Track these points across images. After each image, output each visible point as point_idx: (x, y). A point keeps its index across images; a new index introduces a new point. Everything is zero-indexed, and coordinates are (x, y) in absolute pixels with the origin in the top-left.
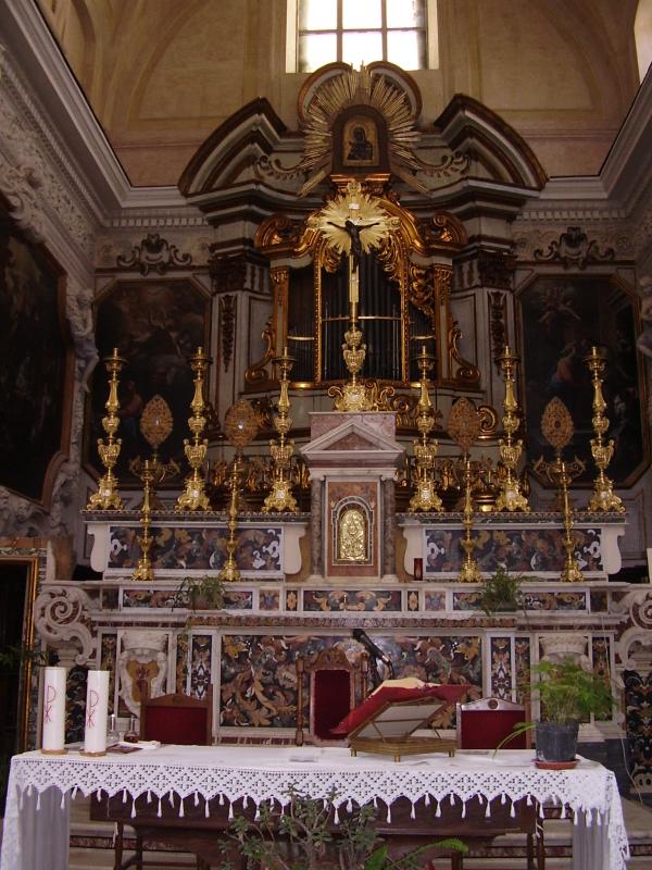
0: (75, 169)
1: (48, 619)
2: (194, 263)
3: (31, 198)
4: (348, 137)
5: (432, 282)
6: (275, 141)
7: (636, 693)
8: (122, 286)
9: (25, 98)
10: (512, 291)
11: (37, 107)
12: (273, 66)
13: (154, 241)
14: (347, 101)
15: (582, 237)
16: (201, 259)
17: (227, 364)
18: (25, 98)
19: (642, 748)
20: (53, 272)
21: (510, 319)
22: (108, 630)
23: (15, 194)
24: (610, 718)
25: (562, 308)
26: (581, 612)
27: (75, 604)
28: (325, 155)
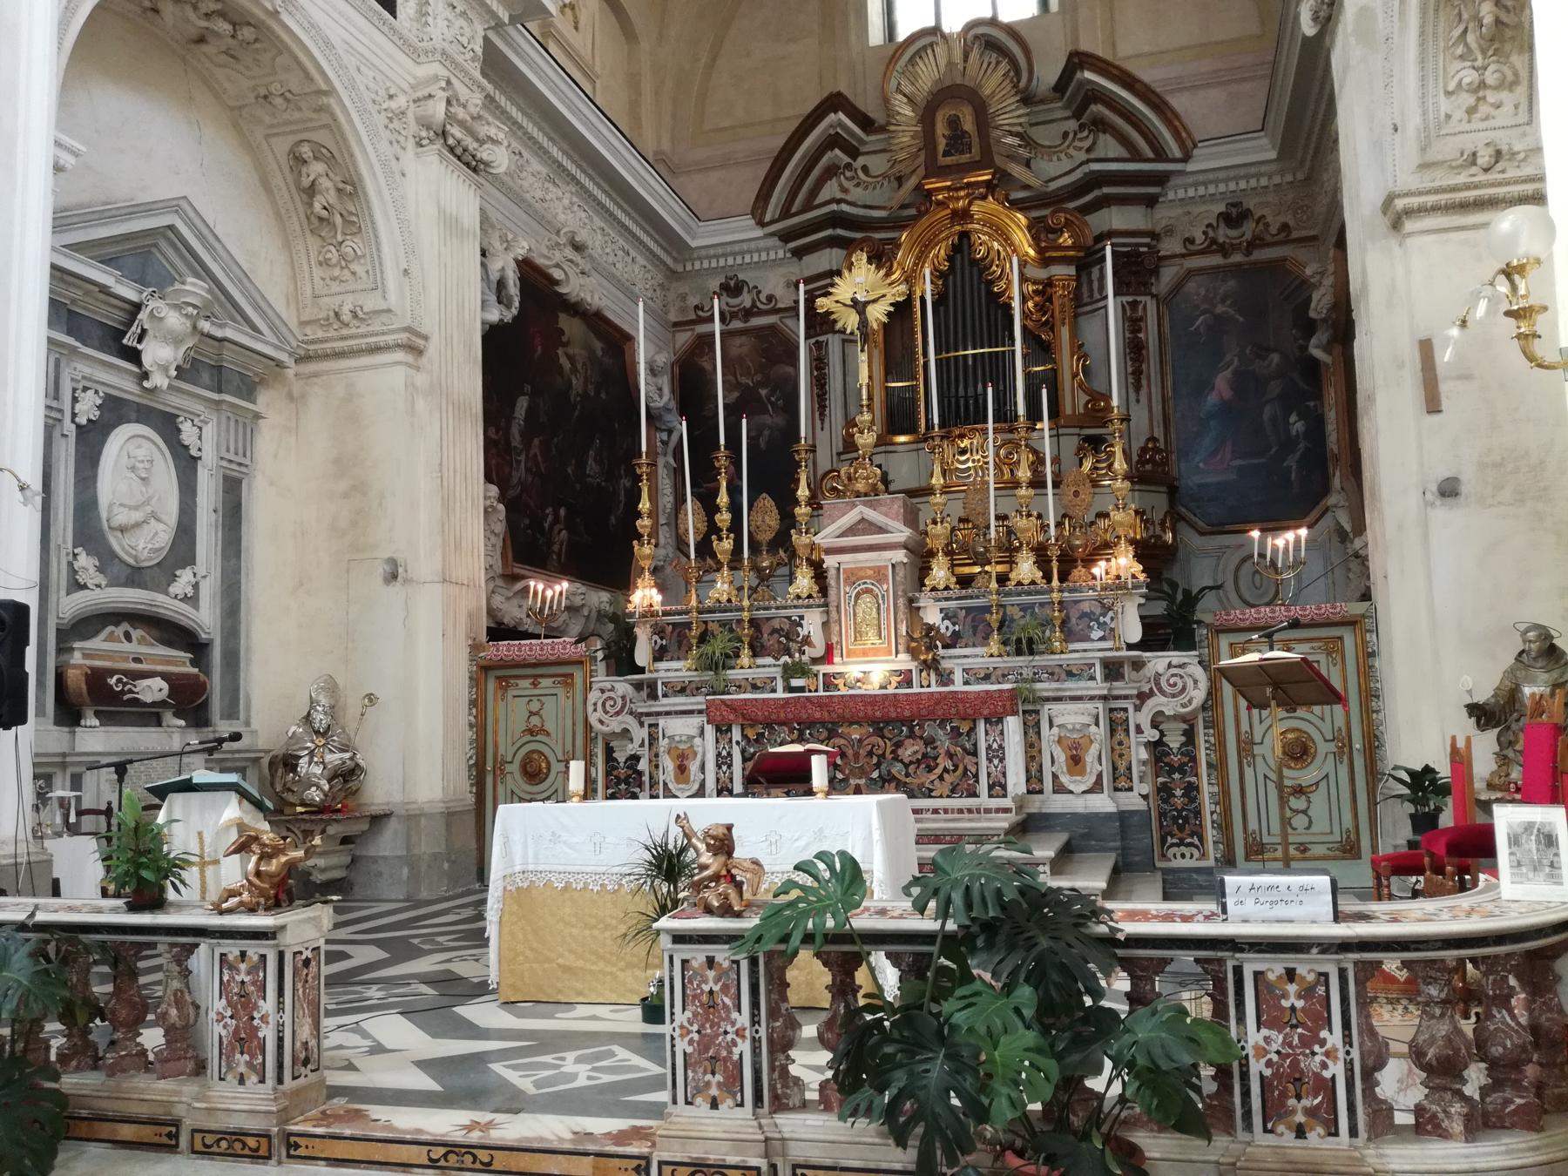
0: (627, 214)
1: (600, 713)
2: (780, 305)
3: (577, 265)
4: (941, 129)
5: (1050, 300)
6: (862, 142)
7: (1167, 764)
9: (554, 151)
10: (1153, 296)
11: (570, 157)
12: (853, 38)
13: (732, 283)
14: (936, 82)
15: (1245, 215)
17: (822, 421)
18: (554, 151)
19: (1175, 819)
20: (617, 341)
21: (1150, 334)
22: (651, 720)
23: (557, 266)
24: (1130, 789)
25: (1220, 309)
26: (1091, 684)
27: (623, 698)
28: (915, 156)
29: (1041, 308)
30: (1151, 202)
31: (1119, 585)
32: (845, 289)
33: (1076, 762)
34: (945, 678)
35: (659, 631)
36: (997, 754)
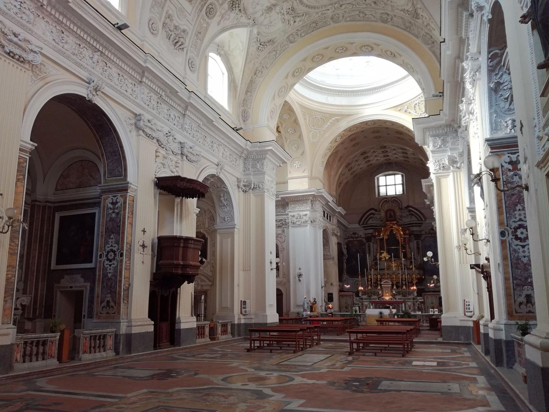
8: (349, 241)
16: (363, 236)
29: (404, 241)
30: (420, 226)
31: (414, 290)
32: (383, 255)
33: (410, 308)
34: (396, 299)
35: (362, 292)
36: (402, 307)
